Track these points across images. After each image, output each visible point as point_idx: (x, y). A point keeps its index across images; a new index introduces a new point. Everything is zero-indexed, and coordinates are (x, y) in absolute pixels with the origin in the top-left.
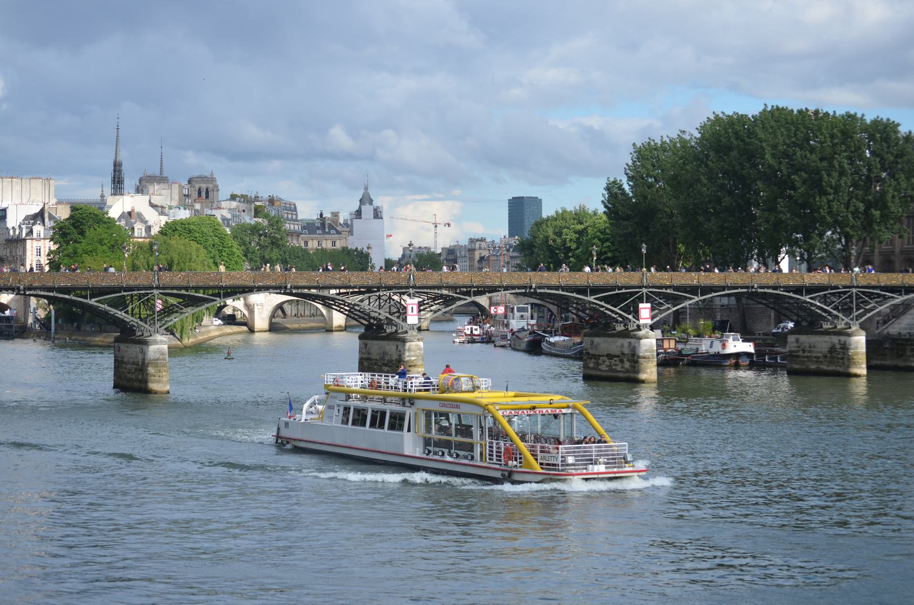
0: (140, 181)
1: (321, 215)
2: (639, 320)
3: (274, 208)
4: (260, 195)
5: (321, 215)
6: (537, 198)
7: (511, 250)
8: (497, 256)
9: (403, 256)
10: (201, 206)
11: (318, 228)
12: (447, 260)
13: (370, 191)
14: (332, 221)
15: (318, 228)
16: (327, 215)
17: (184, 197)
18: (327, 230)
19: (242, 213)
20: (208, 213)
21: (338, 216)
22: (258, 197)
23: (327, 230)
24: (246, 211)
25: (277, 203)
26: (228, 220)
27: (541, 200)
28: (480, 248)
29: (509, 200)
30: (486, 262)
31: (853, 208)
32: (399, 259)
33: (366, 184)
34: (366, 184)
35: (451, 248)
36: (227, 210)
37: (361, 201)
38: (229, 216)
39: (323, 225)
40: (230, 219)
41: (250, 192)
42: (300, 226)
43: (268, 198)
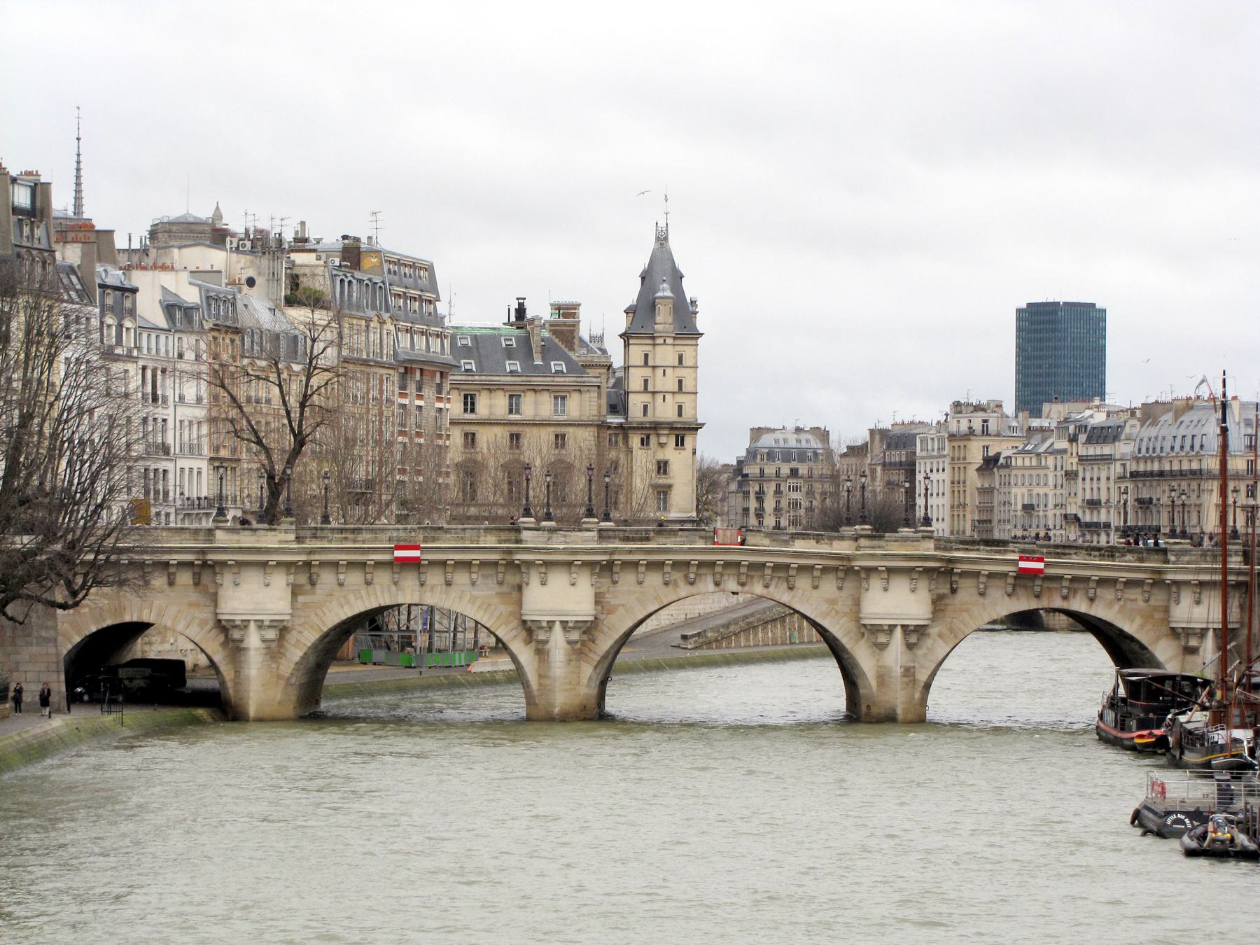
0: (153, 234)
1: (521, 312)
2: (572, 349)
3: (358, 275)
4: (312, 234)
5: (521, 312)
6: (1094, 305)
7: (1082, 438)
8: (1038, 455)
9: (752, 454)
10: (84, 255)
11: (509, 353)
12: (884, 464)
13: (674, 244)
14: (555, 333)
15: (509, 353)
16: (540, 310)
17: (14, 218)
18: (538, 362)
19: (245, 288)
20: (110, 281)
21: (573, 315)
22: (306, 240)
23: (538, 362)
24: (259, 281)
25: (369, 262)
26: (188, 311)
27: (1104, 311)
28: (985, 432)
29: (1019, 311)
30: (1003, 472)
31: (186, 522)
32: (740, 462)
33: (662, 224)
34: (662, 224)
35: (898, 430)
36: (185, 276)
37: (685, 313)
38: (191, 296)
39: (526, 342)
40: (196, 308)
41: (277, 222)
42: (447, 343)
43: (340, 245)
